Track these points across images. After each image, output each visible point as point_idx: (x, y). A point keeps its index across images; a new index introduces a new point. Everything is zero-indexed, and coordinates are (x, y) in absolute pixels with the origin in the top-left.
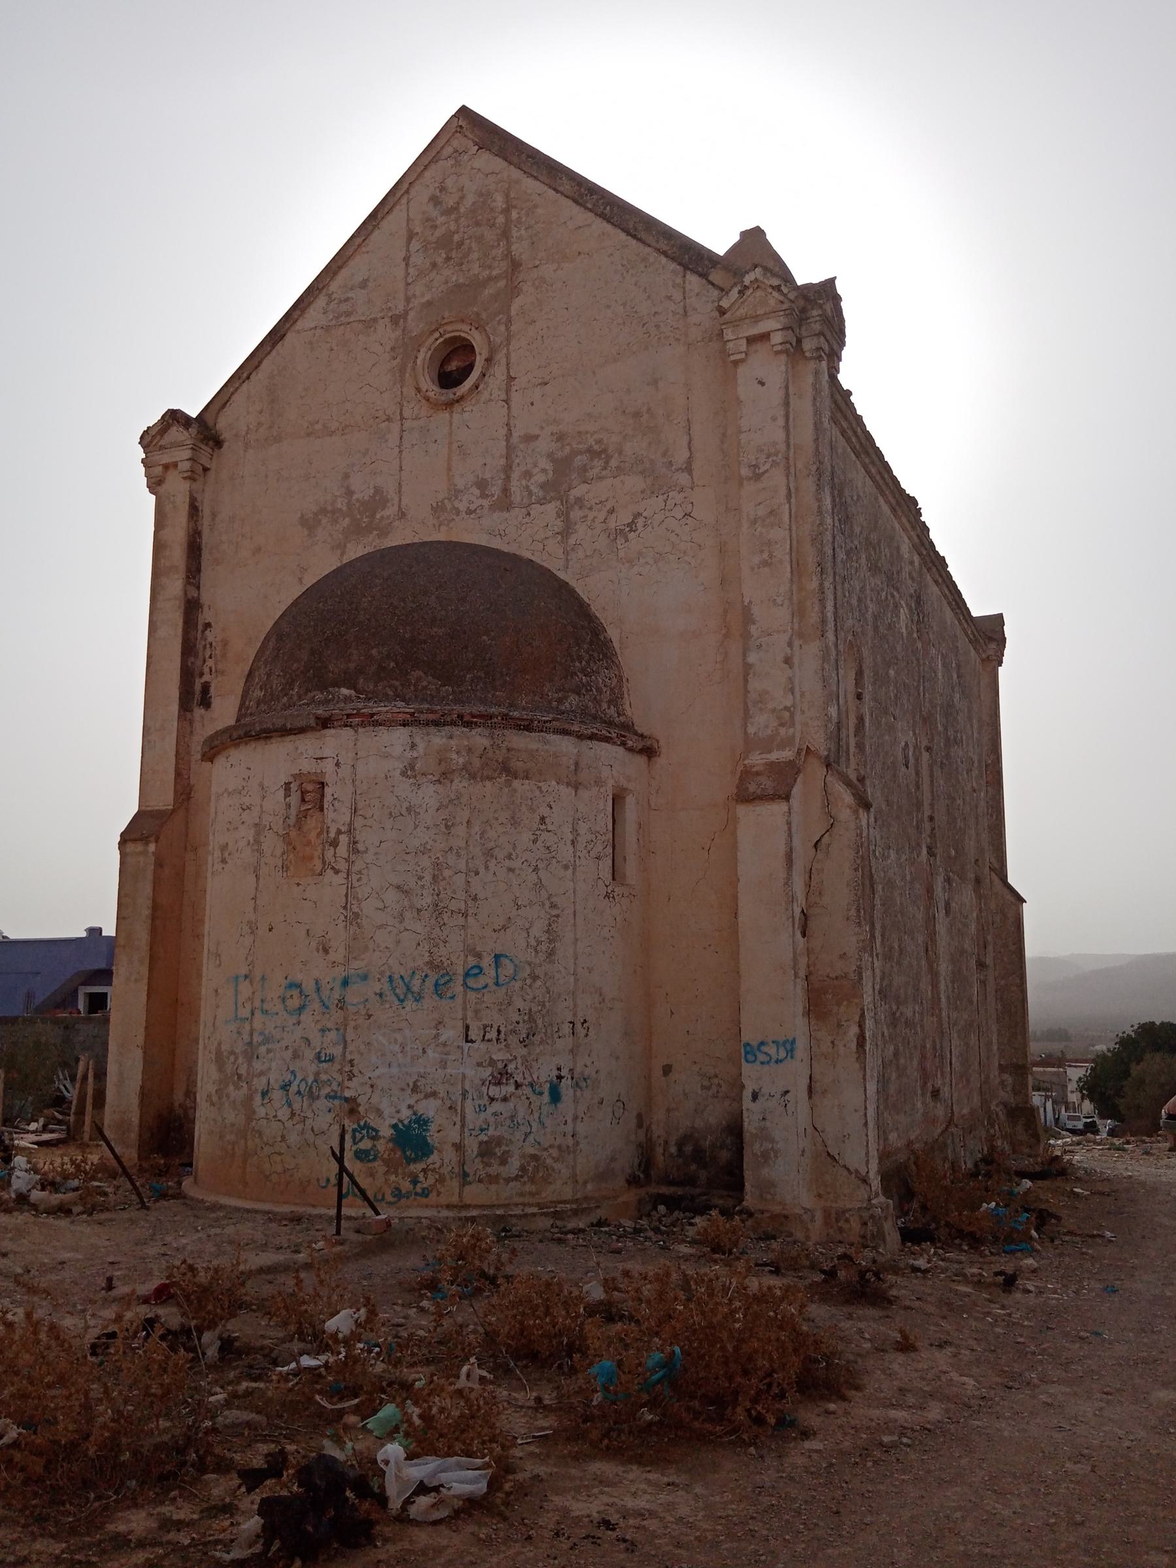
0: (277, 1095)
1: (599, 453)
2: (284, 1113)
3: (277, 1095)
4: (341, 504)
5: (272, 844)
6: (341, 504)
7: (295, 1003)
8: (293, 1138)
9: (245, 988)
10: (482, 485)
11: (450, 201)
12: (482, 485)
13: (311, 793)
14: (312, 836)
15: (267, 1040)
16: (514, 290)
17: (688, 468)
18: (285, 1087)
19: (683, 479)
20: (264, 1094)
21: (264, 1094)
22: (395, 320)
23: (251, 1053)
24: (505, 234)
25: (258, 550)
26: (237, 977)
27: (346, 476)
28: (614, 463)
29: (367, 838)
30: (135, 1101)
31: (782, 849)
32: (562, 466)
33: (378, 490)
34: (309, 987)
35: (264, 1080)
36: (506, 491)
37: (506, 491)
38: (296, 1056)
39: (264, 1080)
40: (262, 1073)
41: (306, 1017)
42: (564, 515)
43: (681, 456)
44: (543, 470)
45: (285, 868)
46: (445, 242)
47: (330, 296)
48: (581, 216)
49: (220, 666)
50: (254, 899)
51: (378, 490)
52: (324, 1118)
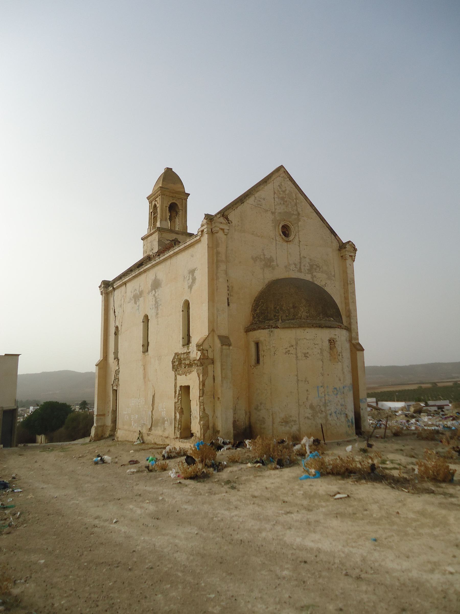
0: (334, 414)
2: (336, 419)
3: (334, 414)
4: (262, 257)
5: (326, 354)
6: (262, 257)
7: (335, 392)
8: (338, 424)
9: (321, 390)
10: (295, 264)
11: (284, 189)
12: (295, 264)
14: (335, 353)
15: (330, 402)
16: (299, 220)
17: (334, 276)
18: (335, 412)
19: (334, 278)
20: (330, 415)
21: (330, 415)
22: (273, 213)
23: (325, 405)
24: (296, 205)
25: (240, 262)
26: (318, 387)
27: (263, 250)
28: (321, 270)
32: (311, 266)
33: (271, 257)
34: (338, 389)
35: (330, 411)
36: (300, 268)
37: (300, 268)
38: (337, 405)
39: (330, 411)
40: (329, 410)
41: (338, 396)
43: (333, 273)
45: (330, 360)
46: (283, 198)
47: (255, 197)
48: (311, 210)
49: (231, 294)
50: (322, 367)
51: (271, 257)
52: (343, 418)
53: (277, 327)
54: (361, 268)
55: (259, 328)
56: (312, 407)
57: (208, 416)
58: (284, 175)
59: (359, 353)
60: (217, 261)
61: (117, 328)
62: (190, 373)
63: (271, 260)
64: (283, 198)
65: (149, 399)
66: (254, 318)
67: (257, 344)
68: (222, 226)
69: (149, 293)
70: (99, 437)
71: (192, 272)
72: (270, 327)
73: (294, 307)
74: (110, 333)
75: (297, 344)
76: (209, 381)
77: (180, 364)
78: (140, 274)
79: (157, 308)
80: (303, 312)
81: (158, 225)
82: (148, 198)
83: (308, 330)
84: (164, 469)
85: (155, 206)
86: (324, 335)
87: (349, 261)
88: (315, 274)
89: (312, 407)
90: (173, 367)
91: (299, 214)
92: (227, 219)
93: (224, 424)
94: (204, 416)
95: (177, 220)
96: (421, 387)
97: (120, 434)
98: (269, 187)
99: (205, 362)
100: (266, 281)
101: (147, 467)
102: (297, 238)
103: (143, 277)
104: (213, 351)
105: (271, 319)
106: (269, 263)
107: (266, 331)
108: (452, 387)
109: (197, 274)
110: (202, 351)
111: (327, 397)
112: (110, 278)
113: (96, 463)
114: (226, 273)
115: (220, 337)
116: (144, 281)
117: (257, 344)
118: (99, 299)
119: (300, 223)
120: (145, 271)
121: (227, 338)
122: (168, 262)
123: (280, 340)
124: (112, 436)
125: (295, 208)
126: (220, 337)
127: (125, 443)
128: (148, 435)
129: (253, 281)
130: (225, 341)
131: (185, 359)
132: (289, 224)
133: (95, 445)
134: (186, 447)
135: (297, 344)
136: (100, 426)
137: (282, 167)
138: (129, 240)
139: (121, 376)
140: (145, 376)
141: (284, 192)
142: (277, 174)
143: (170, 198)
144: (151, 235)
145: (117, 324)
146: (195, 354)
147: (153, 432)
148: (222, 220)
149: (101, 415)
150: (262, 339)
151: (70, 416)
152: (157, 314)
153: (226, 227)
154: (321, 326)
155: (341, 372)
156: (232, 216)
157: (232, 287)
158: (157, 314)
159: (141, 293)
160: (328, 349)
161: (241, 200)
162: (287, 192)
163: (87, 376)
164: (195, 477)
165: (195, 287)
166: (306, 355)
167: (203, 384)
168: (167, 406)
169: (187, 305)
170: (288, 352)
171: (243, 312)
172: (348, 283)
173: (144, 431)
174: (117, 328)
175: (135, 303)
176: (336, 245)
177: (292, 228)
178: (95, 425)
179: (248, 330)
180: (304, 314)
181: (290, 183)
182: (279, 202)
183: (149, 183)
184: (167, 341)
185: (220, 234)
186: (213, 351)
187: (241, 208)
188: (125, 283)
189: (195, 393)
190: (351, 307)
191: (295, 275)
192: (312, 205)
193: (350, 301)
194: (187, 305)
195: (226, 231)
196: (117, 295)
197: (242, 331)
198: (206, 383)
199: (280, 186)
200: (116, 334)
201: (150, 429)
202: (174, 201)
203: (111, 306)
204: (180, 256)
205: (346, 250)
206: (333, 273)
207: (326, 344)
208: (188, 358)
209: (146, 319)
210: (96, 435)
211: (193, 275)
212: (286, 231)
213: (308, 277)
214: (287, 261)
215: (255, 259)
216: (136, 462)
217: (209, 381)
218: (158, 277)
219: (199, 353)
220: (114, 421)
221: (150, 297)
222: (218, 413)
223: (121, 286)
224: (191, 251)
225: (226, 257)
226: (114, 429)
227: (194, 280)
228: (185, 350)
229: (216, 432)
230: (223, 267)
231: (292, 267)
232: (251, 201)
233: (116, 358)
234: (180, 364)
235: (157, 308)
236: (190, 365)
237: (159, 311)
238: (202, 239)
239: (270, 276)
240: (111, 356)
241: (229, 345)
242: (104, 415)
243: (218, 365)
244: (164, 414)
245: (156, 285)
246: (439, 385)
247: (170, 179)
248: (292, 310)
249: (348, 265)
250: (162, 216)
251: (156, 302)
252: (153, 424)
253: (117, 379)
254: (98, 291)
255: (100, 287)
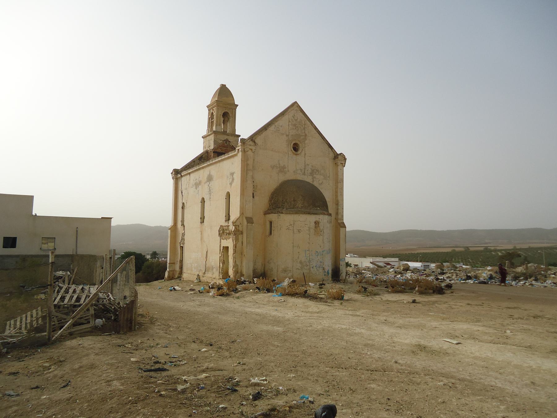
1: (317, 171)
4: (278, 165)
6: (278, 165)
9: (308, 252)
10: (301, 170)
11: (296, 118)
12: (301, 170)
13: (317, 223)
16: (305, 139)
17: (329, 177)
22: (287, 136)
23: (310, 261)
24: (304, 129)
29: (325, 231)
30: (252, 272)
31: (186, 211)
32: (313, 171)
42: (313, 179)
43: (328, 175)
44: (310, 171)
46: (295, 125)
48: (315, 132)
52: (321, 270)
53: (282, 213)
54: (349, 173)
55: (272, 213)
56: (301, 262)
57: (238, 265)
58: (297, 108)
59: (342, 230)
60: (247, 170)
61: (183, 204)
62: (229, 238)
63: (284, 167)
64: (295, 125)
65: (203, 253)
66: (270, 206)
67: (271, 223)
68: (251, 147)
69: (205, 183)
70: (171, 278)
71: (232, 174)
72: (279, 212)
73: (294, 201)
74: (178, 207)
75: (294, 224)
76: (239, 244)
77: (223, 232)
78: (199, 169)
79: (210, 194)
80: (299, 204)
81: (214, 129)
82: (208, 107)
83: (301, 215)
84: (208, 292)
85: (212, 113)
86: (312, 219)
87: (340, 167)
88: (315, 176)
89: (301, 262)
90: (219, 235)
91: (306, 135)
92: (254, 142)
93: (247, 269)
94: (235, 266)
95: (228, 124)
96: (454, 250)
97: (185, 276)
98: (286, 117)
99: (237, 233)
100: (280, 182)
101: (199, 291)
102: (304, 152)
103: (202, 171)
104: (242, 226)
105: (279, 208)
106: (282, 170)
107: (277, 214)
108: (481, 251)
109: (235, 176)
110: (235, 226)
111: (311, 257)
112: (179, 167)
113: (171, 290)
114: (253, 178)
115: (246, 218)
116: (201, 174)
117: (271, 223)
118: (171, 182)
119: (306, 142)
120: (203, 168)
121: (251, 218)
122: (218, 164)
123: (285, 221)
124: (180, 277)
125: (303, 131)
126: (246, 218)
127: (189, 282)
128: (203, 277)
129: (270, 181)
130: (250, 220)
131: (226, 230)
132: (298, 143)
133: (168, 282)
134: (287, 317)
135: (294, 224)
136: (172, 271)
137: (296, 102)
138: (193, 139)
139: (186, 237)
140: (202, 239)
141: (296, 120)
142: (292, 108)
143: (224, 107)
144: (209, 135)
145: (184, 201)
146: (232, 228)
147: (206, 275)
148: (251, 143)
149: (172, 263)
150: (273, 219)
151: (146, 264)
152: (210, 198)
153: (253, 148)
154: (309, 213)
155: (324, 242)
156: (258, 140)
157: (257, 186)
158: (210, 198)
159: (200, 183)
160: (313, 228)
161: (265, 128)
162: (299, 120)
163: (158, 230)
164: (222, 295)
165: (233, 184)
166: (299, 231)
167: (235, 246)
168: (215, 259)
169: (228, 195)
170: (288, 229)
171: (263, 201)
172: (338, 182)
173: (201, 274)
174: (183, 204)
175: (196, 188)
176: (332, 155)
177: (300, 145)
178: (168, 270)
179: (266, 213)
180: (300, 206)
181: (301, 114)
182: (294, 127)
183: (208, 96)
184: (216, 217)
185: (250, 153)
186: (242, 226)
187: (265, 133)
188: (189, 174)
189: (231, 251)
190: (339, 198)
191: (300, 177)
192: (316, 128)
193: (339, 194)
194: (228, 195)
195: (253, 150)
196: (184, 181)
197: (262, 213)
198: (238, 245)
199: (293, 117)
200: (183, 208)
201: (204, 273)
202: (227, 111)
203: (180, 188)
204: (225, 162)
205: (339, 159)
206: (328, 175)
207: (313, 224)
208: (228, 229)
209: (203, 201)
210: (169, 277)
211: (232, 176)
212: (296, 148)
213: (308, 179)
214: (295, 168)
215: (273, 167)
216: (194, 290)
217: (239, 244)
218: (211, 173)
219: (234, 227)
220: (181, 268)
221: (206, 186)
222: (244, 264)
223: (186, 175)
224: (232, 160)
225: (253, 167)
226: (181, 273)
227: (233, 179)
228: (227, 224)
229: (242, 275)
230: (250, 174)
231: (299, 172)
232: (272, 128)
233: (183, 225)
234: (223, 232)
235: (210, 194)
236: (229, 234)
237: (212, 197)
238: (238, 154)
239: (283, 178)
240: (179, 223)
241: (252, 223)
242: (174, 263)
243: (245, 235)
244: (213, 264)
245: (210, 179)
246: (471, 249)
247: (224, 93)
248: (293, 202)
249: (339, 170)
250: (217, 122)
251: (210, 190)
252: (206, 270)
253: (183, 239)
254: (170, 177)
255: (172, 173)
